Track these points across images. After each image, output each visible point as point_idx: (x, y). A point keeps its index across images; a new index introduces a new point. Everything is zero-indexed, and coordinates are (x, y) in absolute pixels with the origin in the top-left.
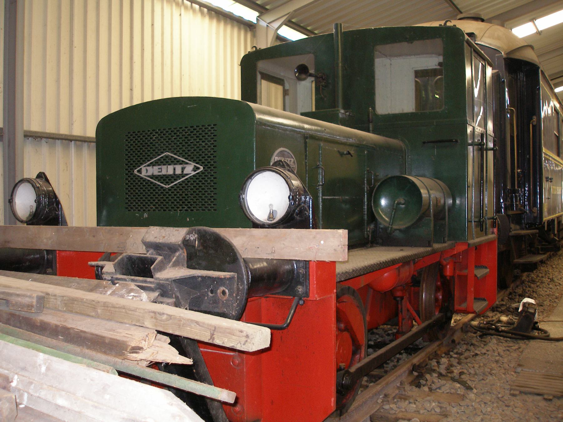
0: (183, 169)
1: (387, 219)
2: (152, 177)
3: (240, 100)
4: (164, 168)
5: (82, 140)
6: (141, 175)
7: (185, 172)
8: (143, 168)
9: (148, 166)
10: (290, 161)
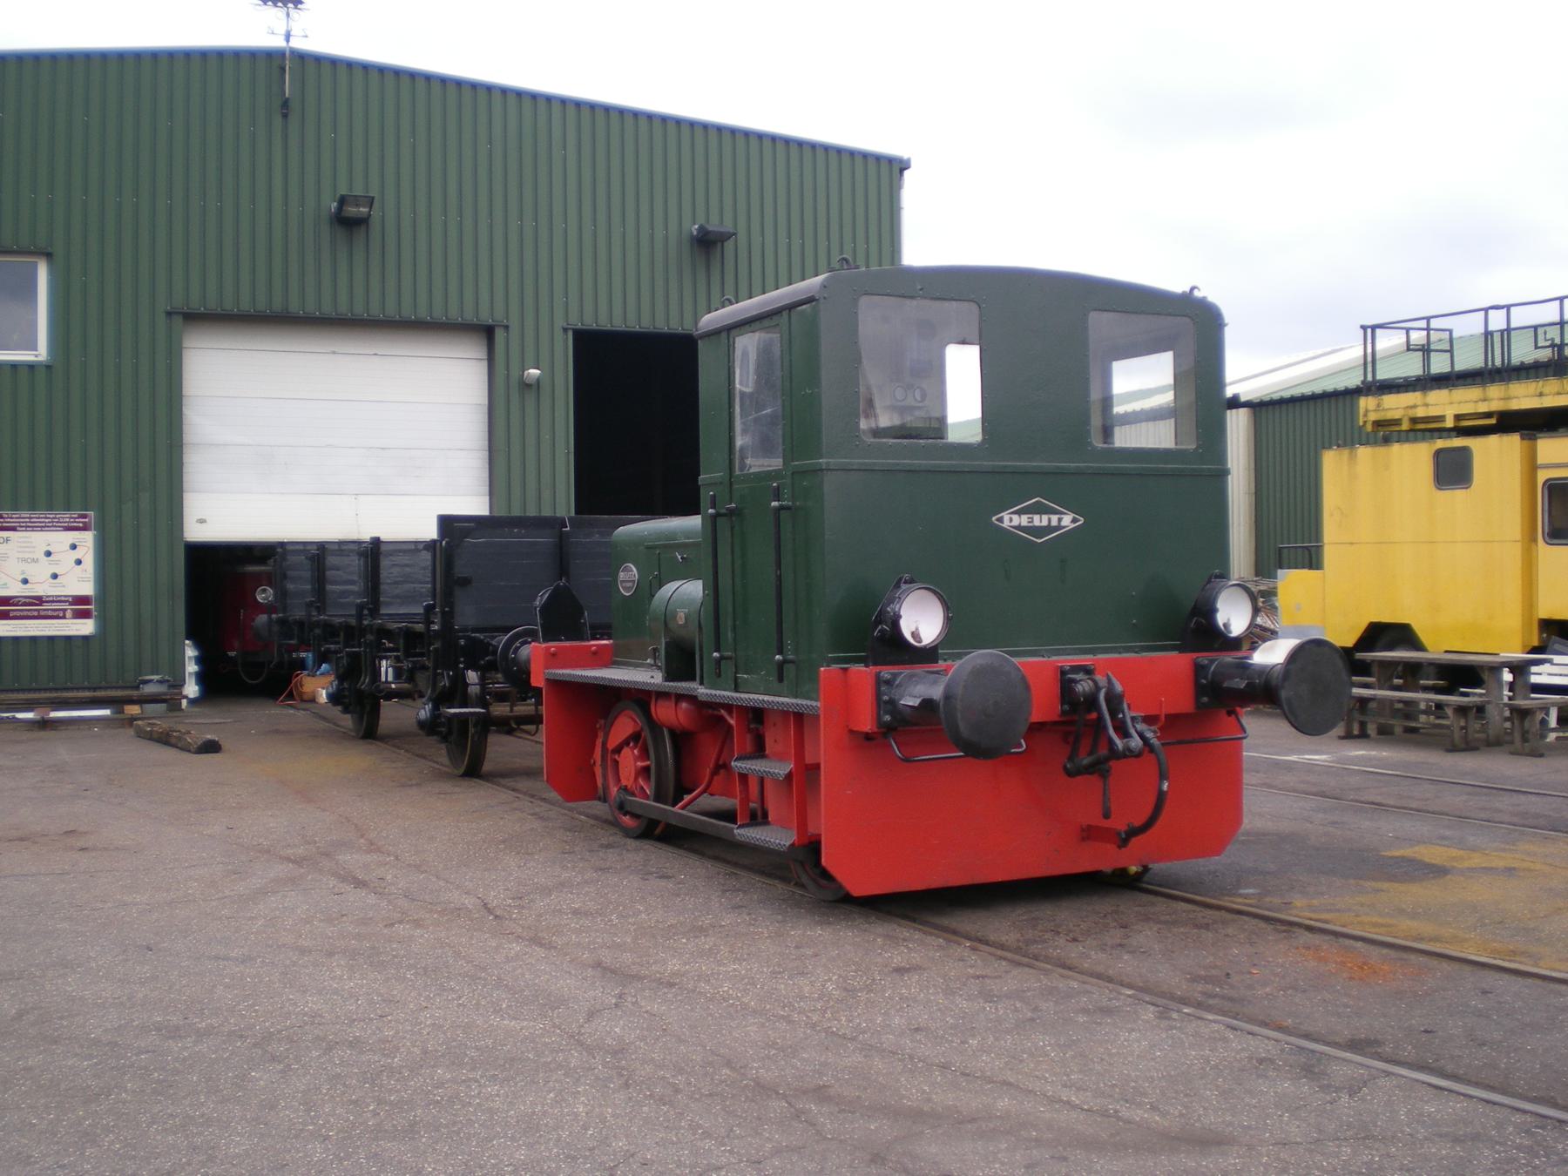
0: (1060, 520)
1: (456, 524)
2: (1019, 528)
3: (700, 516)
4: (1036, 518)
5: (555, 513)
6: (1004, 525)
7: (1063, 524)
8: (1006, 516)
9: (1012, 513)
10: (1011, 520)
